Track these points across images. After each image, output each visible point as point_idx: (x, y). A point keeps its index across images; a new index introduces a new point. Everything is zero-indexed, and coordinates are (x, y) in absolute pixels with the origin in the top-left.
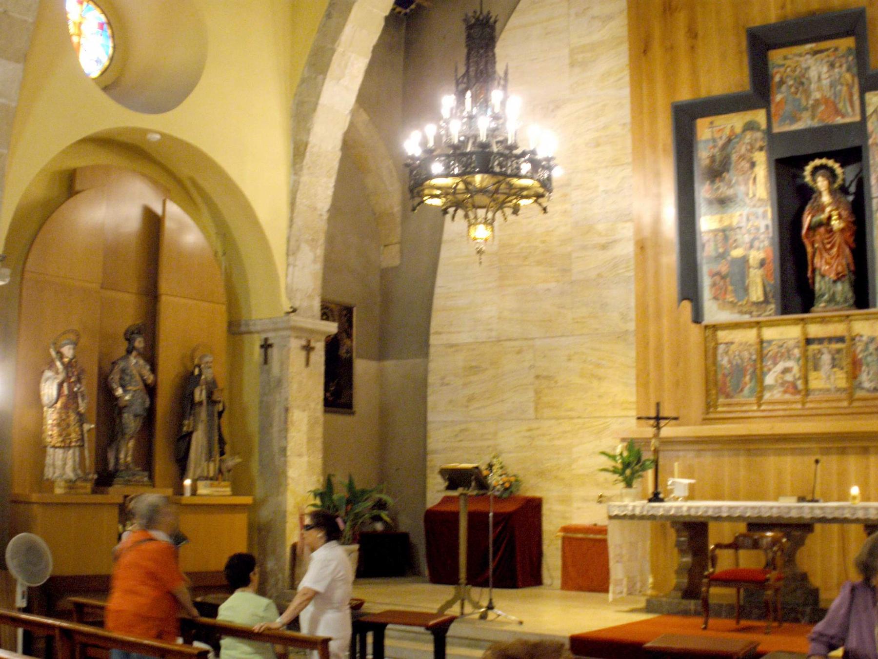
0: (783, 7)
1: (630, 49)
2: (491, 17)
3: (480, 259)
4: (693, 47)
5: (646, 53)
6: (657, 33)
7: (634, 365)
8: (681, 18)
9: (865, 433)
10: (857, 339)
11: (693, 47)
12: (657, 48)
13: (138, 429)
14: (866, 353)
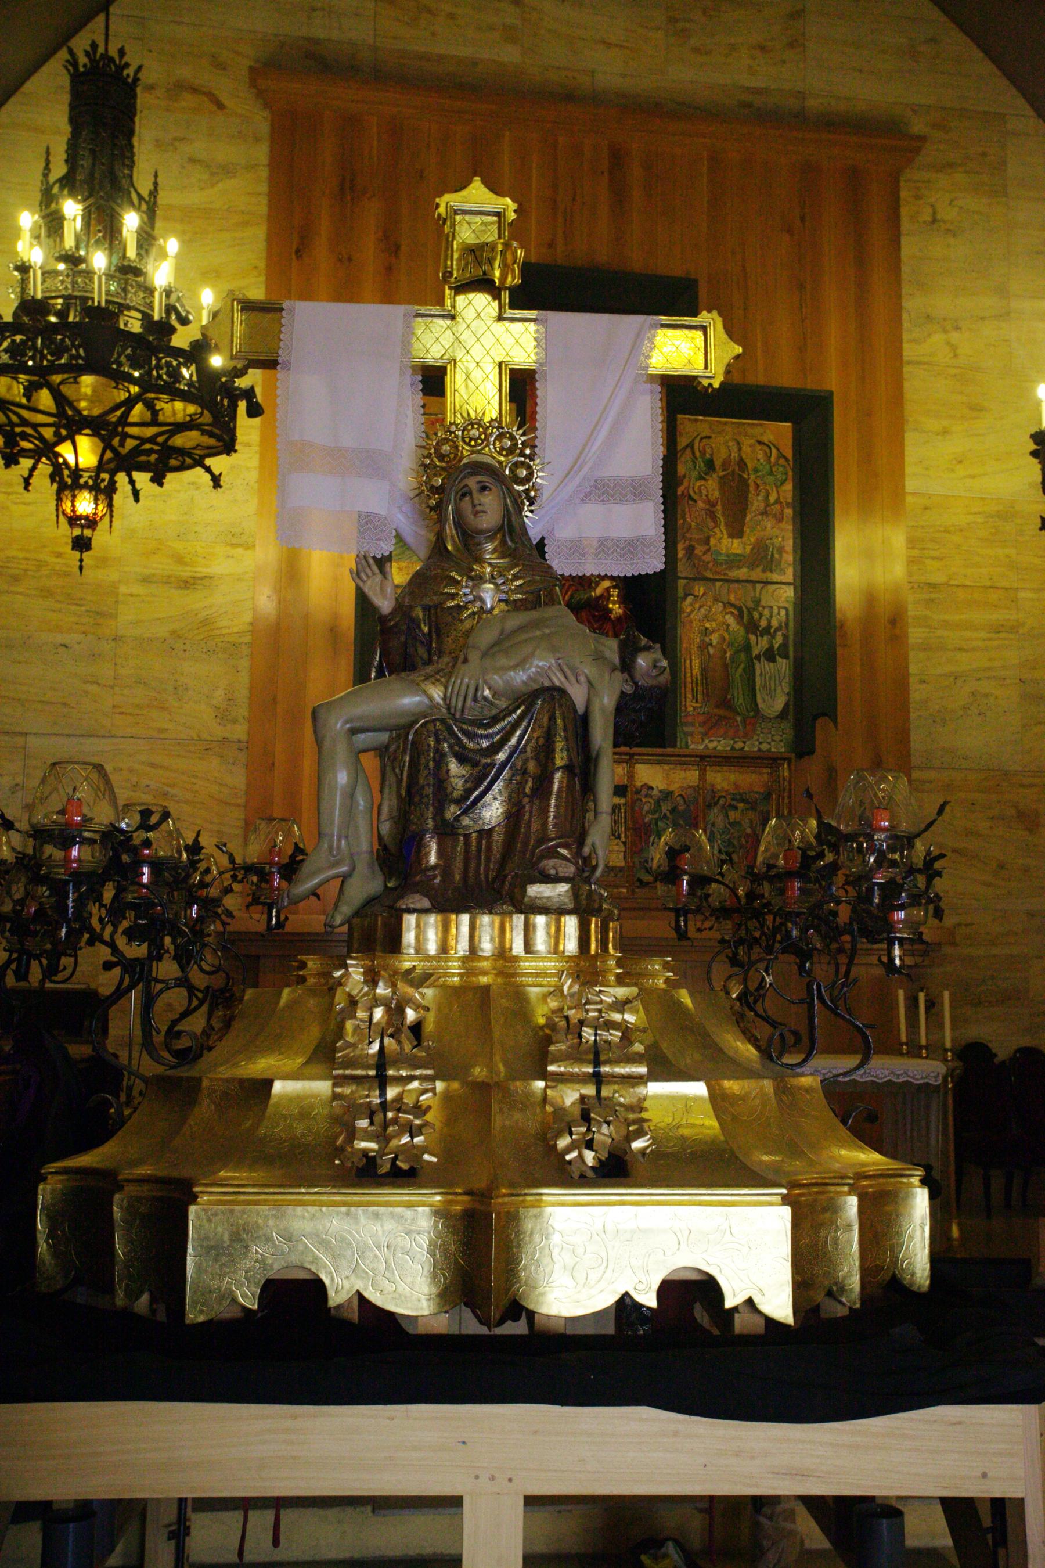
0: (551, 245)
1: (270, 240)
2: (127, 65)
3: (81, 560)
4: (389, 269)
5: (301, 256)
6: (324, 227)
7: (906, 369)
8: (372, 211)
9: (298, 1498)
10: (644, 791)
11: (389, 269)
12: (321, 252)
13: (448, 378)
14: (656, 816)
